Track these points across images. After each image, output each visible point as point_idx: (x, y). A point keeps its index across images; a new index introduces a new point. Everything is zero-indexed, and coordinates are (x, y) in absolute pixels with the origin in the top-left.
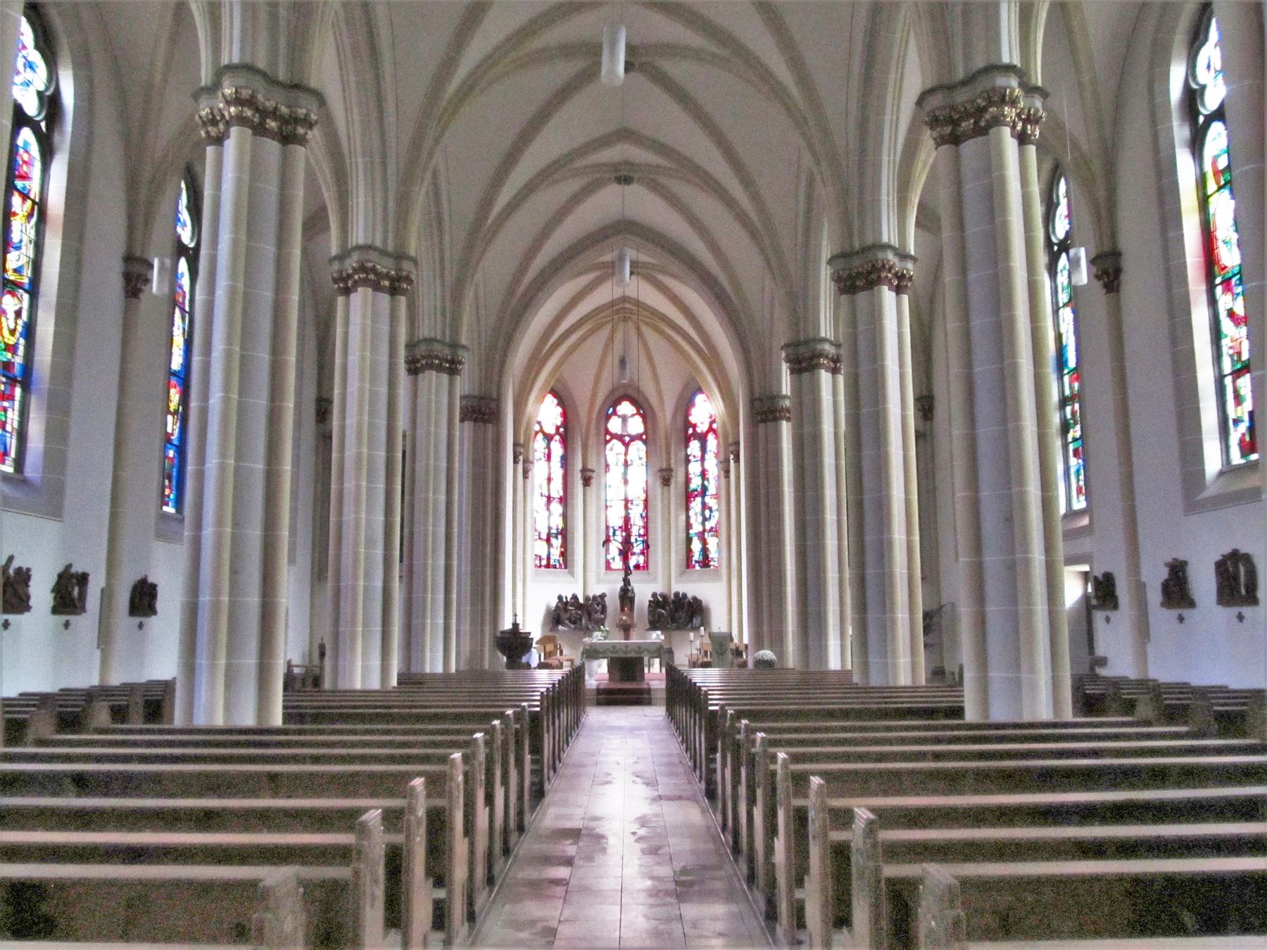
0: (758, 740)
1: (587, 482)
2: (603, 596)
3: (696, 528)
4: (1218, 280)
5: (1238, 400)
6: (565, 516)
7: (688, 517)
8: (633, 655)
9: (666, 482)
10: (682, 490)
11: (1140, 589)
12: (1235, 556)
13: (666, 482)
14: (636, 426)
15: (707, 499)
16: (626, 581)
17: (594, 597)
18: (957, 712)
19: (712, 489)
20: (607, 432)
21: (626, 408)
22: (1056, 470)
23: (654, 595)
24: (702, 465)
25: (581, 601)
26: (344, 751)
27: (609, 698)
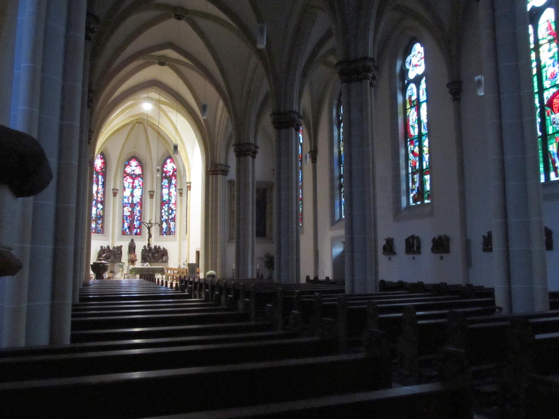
1: (115, 194)
2: (121, 247)
3: (165, 217)
4: (409, 140)
5: (414, 182)
7: (161, 213)
8: (151, 273)
9: (152, 196)
11: (467, 245)
12: (413, 237)
13: (152, 196)
14: (138, 171)
15: (171, 205)
18: (343, 291)
19: (173, 201)
20: (125, 172)
21: (134, 163)
24: (169, 190)
25: (111, 248)
26: (104, 307)
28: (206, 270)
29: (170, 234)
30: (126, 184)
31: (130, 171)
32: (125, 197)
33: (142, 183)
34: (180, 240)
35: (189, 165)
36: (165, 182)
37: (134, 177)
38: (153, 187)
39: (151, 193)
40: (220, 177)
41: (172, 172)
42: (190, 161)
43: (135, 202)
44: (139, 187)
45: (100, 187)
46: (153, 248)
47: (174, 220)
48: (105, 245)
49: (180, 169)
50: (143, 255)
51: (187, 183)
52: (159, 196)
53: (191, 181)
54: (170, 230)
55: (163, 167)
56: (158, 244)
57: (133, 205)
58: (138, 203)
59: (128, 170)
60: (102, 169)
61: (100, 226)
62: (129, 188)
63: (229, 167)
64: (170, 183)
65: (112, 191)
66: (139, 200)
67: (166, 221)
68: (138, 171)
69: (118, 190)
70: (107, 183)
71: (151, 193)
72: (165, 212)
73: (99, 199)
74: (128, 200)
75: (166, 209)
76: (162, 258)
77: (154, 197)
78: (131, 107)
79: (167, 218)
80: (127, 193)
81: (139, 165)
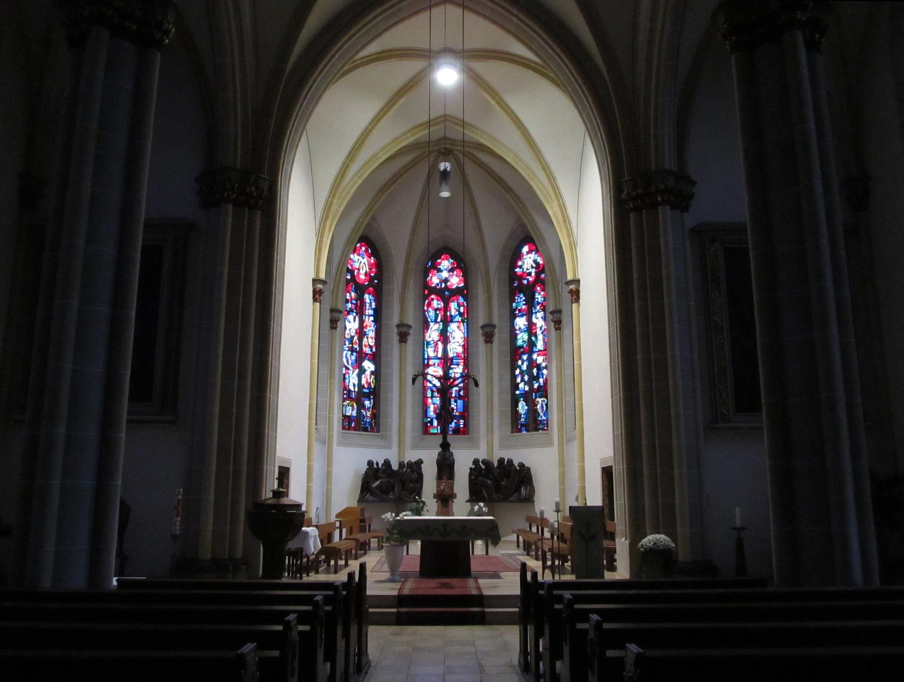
0: (630, 661)
1: (403, 338)
2: (420, 462)
7: (514, 377)
9: (489, 338)
10: (507, 348)
13: (489, 338)
14: (455, 281)
15: (535, 356)
16: (445, 446)
17: (410, 464)
19: (540, 345)
20: (426, 285)
23: (476, 462)
24: (529, 320)
25: (395, 467)
27: (412, 611)
28: (637, 532)
29: (537, 429)
30: (431, 314)
32: (428, 343)
34: (561, 445)
35: (570, 234)
36: (520, 302)
37: (446, 294)
38: (490, 316)
39: (487, 329)
40: (665, 214)
41: (533, 271)
42: (574, 225)
43: (451, 355)
44: (459, 318)
45: (369, 321)
46: (496, 465)
47: (543, 391)
48: (379, 457)
49: (553, 269)
51: (569, 283)
52: (507, 336)
53: (580, 276)
54: (535, 420)
55: (514, 265)
56: (506, 455)
58: (458, 356)
60: (371, 279)
61: (369, 414)
62: (436, 322)
63: (693, 183)
64: (531, 302)
65: (395, 330)
66: (460, 350)
67: (527, 396)
68: (455, 281)
69: (410, 327)
71: (487, 329)
72: (522, 373)
73: (367, 350)
74: (436, 351)
75: (524, 368)
76: (518, 490)
77: (496, 339)
78: (409, 90)
79: (527, 388)
80: (433, 334)
81: (459, 267)
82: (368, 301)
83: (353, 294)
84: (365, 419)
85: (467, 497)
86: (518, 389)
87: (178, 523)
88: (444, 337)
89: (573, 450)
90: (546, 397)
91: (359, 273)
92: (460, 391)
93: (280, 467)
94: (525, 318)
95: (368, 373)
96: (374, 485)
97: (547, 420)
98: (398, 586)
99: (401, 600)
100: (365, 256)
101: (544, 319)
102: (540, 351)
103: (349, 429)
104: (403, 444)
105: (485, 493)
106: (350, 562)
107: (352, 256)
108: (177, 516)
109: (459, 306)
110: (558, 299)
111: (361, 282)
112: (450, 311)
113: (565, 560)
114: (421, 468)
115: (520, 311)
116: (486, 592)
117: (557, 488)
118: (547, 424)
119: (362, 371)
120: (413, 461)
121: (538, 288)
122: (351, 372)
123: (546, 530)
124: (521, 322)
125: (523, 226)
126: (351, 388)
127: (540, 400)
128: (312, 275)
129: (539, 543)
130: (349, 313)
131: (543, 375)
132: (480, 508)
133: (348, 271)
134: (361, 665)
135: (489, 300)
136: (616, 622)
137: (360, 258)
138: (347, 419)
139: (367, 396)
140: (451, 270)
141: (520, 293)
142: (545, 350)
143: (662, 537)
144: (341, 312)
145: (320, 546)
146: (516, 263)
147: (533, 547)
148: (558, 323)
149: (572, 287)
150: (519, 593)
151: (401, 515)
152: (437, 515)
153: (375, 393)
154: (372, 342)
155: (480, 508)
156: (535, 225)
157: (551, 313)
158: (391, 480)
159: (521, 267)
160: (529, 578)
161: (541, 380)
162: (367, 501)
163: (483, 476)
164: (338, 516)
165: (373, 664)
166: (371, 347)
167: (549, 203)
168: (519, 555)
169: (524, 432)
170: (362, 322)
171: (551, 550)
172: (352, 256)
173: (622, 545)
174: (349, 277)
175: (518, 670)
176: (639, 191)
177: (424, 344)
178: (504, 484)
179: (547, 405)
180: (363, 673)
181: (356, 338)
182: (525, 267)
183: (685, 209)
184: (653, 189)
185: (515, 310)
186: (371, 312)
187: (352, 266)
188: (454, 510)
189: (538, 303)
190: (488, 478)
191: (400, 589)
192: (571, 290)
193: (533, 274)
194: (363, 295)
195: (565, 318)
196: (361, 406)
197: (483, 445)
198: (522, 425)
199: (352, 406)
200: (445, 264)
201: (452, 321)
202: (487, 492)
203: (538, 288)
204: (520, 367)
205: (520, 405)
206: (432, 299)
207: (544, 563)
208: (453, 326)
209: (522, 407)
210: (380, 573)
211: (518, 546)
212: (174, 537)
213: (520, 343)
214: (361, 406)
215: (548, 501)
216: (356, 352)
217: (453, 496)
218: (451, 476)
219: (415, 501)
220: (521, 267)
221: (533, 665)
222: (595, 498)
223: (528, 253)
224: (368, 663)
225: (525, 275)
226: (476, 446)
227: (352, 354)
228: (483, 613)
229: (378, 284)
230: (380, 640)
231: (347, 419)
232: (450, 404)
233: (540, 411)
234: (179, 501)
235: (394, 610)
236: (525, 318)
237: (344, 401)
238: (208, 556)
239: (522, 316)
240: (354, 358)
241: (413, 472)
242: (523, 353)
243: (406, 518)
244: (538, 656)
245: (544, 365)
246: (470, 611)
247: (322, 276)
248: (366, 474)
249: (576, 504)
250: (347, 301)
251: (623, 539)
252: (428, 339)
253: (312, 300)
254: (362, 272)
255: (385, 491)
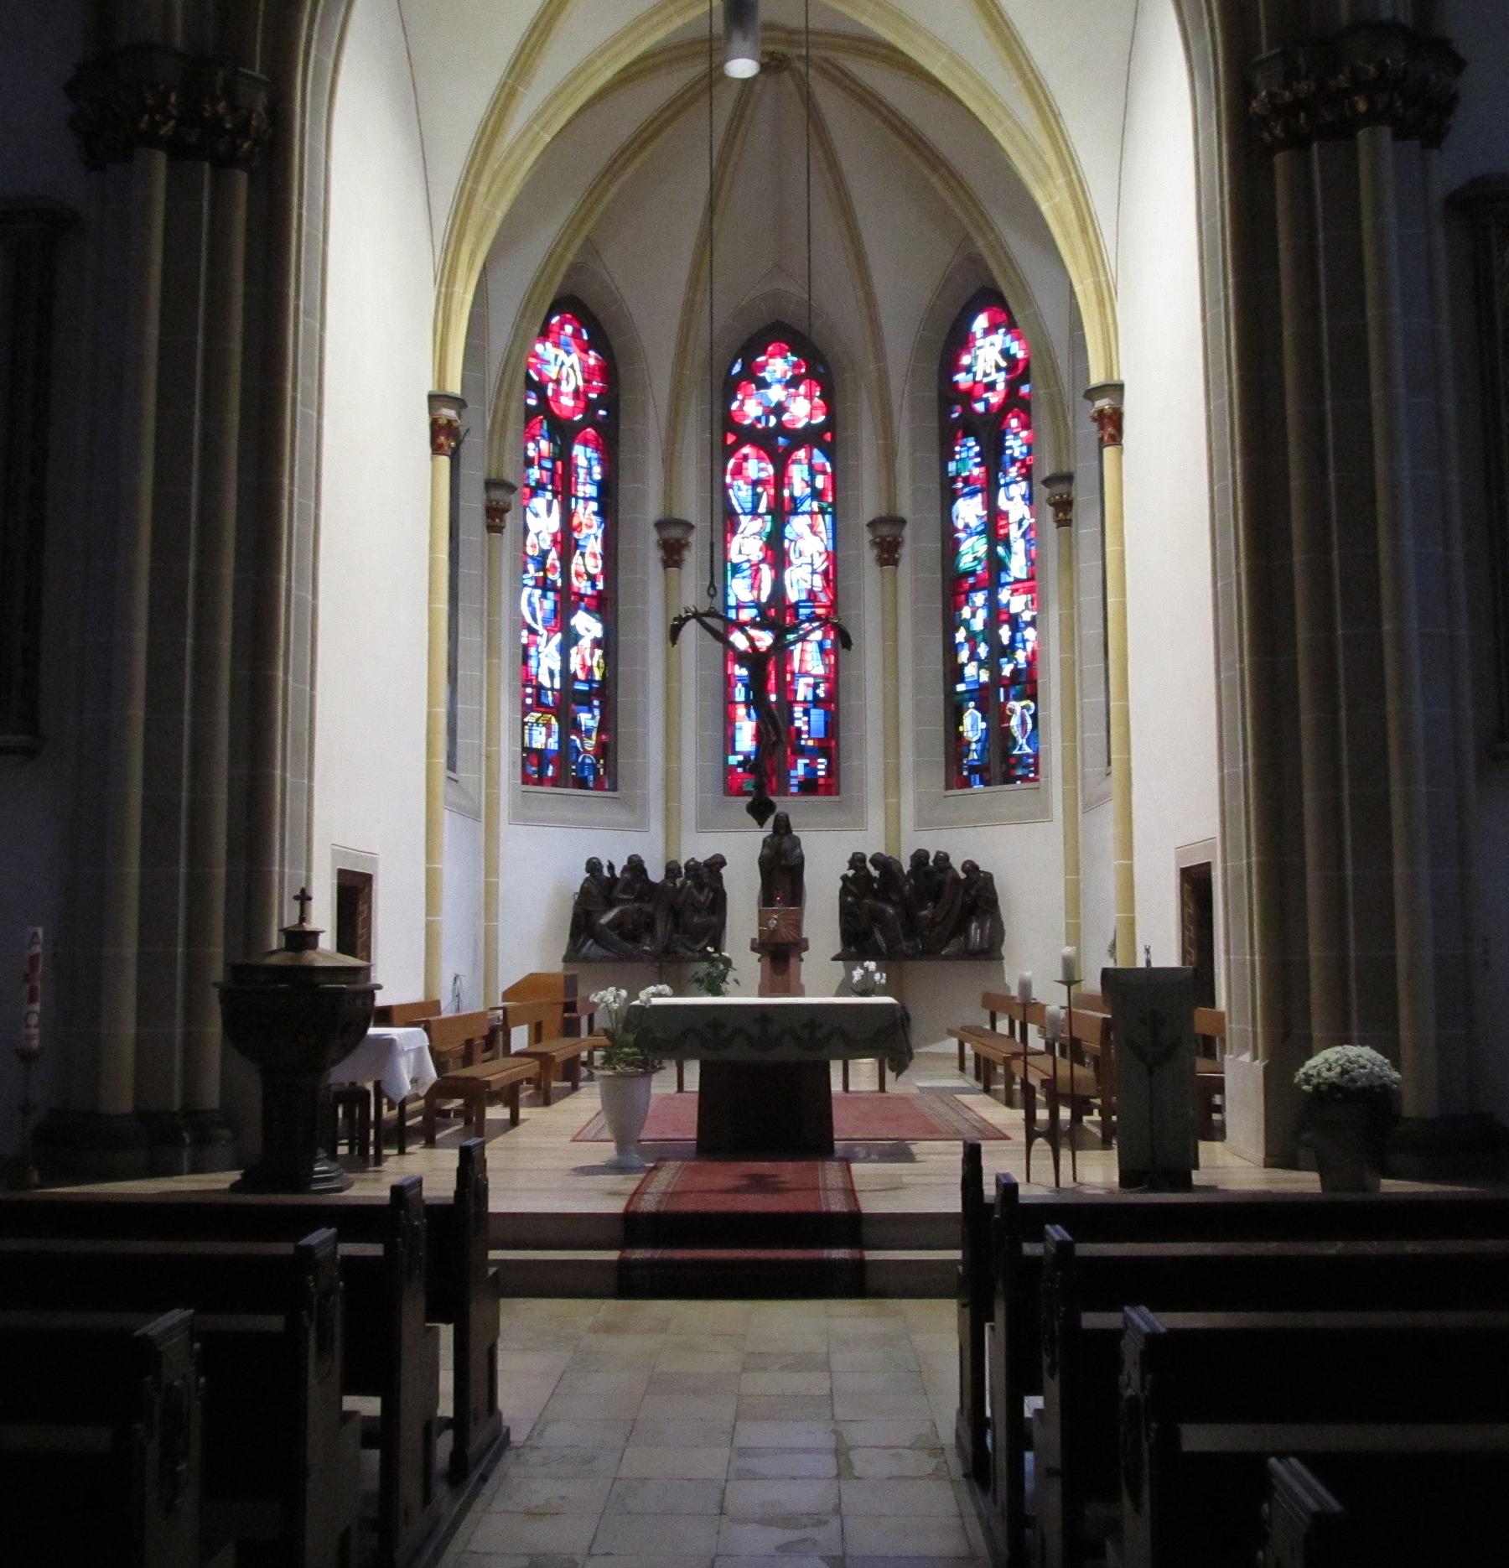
1: (672, 553)
2: (717, 863)
6: (607, 644)
7: (951, 649)
8: (787, 1052)
9: (888, 552)
13: (888, 552)
14: (802, 410)
15: (1004, 595)
17: (693, 868)
19: (1018, 567)
20: (729, 422)
22: (1430, 1193)
23: (857, 861)
25: (656, 874)
27: (661, 1255)
28: (1286, 1041)
29: (1009, 779)
30: (740, 494)
31: (759, 411)
32: (736, 569)
33: (834, 477)
36: (968, 457)
37: (777, 443)
39: (885, 530)
40: (1377, 149)
41: (1001, 379)
42: (1108, 241)
43: (793, 595)
45: (586, 514)
47: (1026, 683)
48: (615, 851)
50: (846, 912)
52: (934, 546)
53: (1124, 375)
55: (950, 365)
56: (933, 843)
57: (778, 615)
59: (751, 409)
60: (589, 407)
61: (590, 744)
62: (754, 513)
63: (1459, 65)
64: (994, 457)
65: (654, 536)
67: (984, 697)
68: (802, 410)
69: (689, 527)
70: (625, 486)
71: (885, 530)
72: (972, 638)
73: (582, 586)
75: (978, 624)
76: (962, 929)
77: (906, 553)
79: (984, 677)
80: (747, 544)
82: (582, 462)
83: (544, 445)
84: (581, 759)
85: (837, 948)
86: (962, 679)
87: (34, 1020)
88: (777, 553)
89: (1103, 827)
90: (1033, 697)
91: (557, 393)
92: (816, 686)
93: (343, 874)
94: (979, 498)
95: (585, 643)
96: (604, 920)
97: (1036, 756)
98: (630, 1183)
99: (633, 1227)
100: (573, 348)
101: (1029, 499)
102: (1017, 581)
103: (541, 781)
104: (676, 820)
105: (879, 937)
106: (524, 1113)
107: (539, 348)
108: (32, 1000)
109: (813, 471)
110: (1064, 443)
111: (565, 413)
112: (790, 484)
113: (1081, 1107)
114: (720, 878)
115: (966, 481)
116: (871, 1205)
117: (1061, 923)
118: (1036, 764)
119: (570, 639)
120: (701, 859)
121: (1014, 423)
122: (541, 640)
123: (1032, 1029)
124: (969, 511)
125: (975, 262)
126: (545, 680)
127: (1016, 705)
128: (429, 386)
129: (1018, 1066)
130: (534, 493)
131: (1024, 641)
132: (868, 973)
133: (530, 384)
134: (477, 1443)
135: (888, 456)
136: (1257, 1308)
137: (562, 354)
138: (533, 759)
139: (585, 700)
140: (792, 383)
141: (966, 435)
142: (1031, 578)
143: (1362, 1054)
144: (511, 488)
145: (432, 1075)
146: (958, 358)
147: (1000, 1070)
148: (1064, 508)
149: (1103, 403)
150: (959, 1210)
151: (643, 995)
152: (761, 995)
153: (604, 693)
154: (594, 566)
155: (868, 973)
156: (1009, 261)
157: (1047, 482)
158: (648, 908)
159: (968, 369)
160: (990, 1190)
161: (1021, 656)
162: (587, 959)
163: (875, 895)
164: (507, 995)
165: (517, 1437)
166: (592, 579)
167: (1038, 179)
168: (962, 1091)
169: (978, 787)
170: (567, 515)
171: (1050, 1085)
172: (539, 348)
173: (1242, 1075)
174: (532, 402)
175: (956, 1467)
176: (1304, 87)
177: (719, 570)
178: (928, 914)
179: (1034, 717)
180: (475, 1477)
181: (553, 555)
182: (979, 370)
183: (1434, 138)
184: (1343, 80)
185: (954, 480)
186: (592, 491)
187: (539, 372)
188: (804, 979)
189: (1013, 460)
190: (888, 901)
191: (637, 1193)
192: (1101, 411)
193: (1001, 386)
194: (570, 449)
195: (1082, 495)
196: (570, 726)
197: (875, 817)
198: (973, 769)
199: (548, 725)
200: (778, 367)
201: (795, 512)
202: (882, 931)
203: (1014, 423)
204: (966, 624)
205: (968, 719)
206: (745, 458)
207: (1030, 1119)
208: (798, 525)
209: (973, 725)
210: (553, 1161)
211: (962, 1068)
212: (27, 1057)
213: (966, 562)
214: (570, 726)
215: (1043, 953)
216: (554, 589)
217: (800, 945)
218: (795, 895)
219: (707, 957)
220: (968, 369)
221: (1001, 1463)
222: (1161, 945)
223: (988, 332)
224: (500, 1441)
225: (979, 388)
226: (859, 823)
227: (544, 596)
228: (861, 1265)
229: (607, 417)
230: (543, 1359)
231: (533, 759)
232: (792, 720)
233: (1016, 732)
234: (34, 959)
235: (613, 1255)
236: (979, 498)
237: (525, 714)
238: (126, 1105)
239: (972, 494)
240: (549, 605)
241: (700, 887)
242: (974, 588)
243: (656, 1001)
244: (1020, 1434)
245: (1027, 616)
246: (822, 1257)
247: (454, 387)
248: (584, 892)
249: (1110, 964)
250: (529, 462)
251: (1246, 1057)
252: (734, 557)
253: (428, 449)
254: (567, 388)
255: (630, 932)
